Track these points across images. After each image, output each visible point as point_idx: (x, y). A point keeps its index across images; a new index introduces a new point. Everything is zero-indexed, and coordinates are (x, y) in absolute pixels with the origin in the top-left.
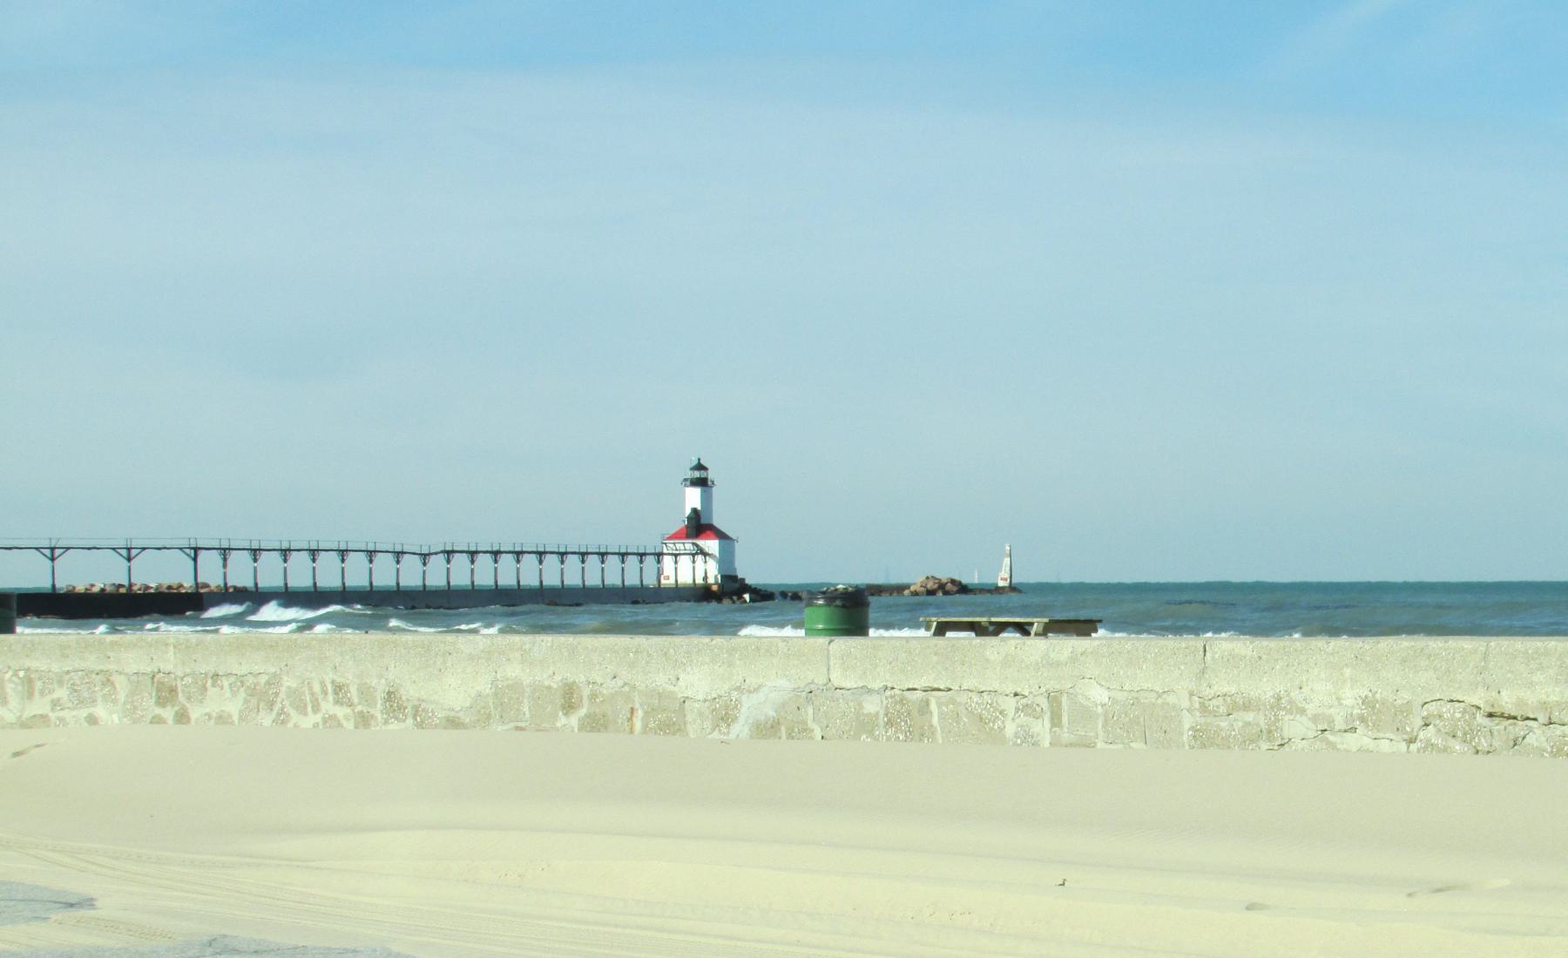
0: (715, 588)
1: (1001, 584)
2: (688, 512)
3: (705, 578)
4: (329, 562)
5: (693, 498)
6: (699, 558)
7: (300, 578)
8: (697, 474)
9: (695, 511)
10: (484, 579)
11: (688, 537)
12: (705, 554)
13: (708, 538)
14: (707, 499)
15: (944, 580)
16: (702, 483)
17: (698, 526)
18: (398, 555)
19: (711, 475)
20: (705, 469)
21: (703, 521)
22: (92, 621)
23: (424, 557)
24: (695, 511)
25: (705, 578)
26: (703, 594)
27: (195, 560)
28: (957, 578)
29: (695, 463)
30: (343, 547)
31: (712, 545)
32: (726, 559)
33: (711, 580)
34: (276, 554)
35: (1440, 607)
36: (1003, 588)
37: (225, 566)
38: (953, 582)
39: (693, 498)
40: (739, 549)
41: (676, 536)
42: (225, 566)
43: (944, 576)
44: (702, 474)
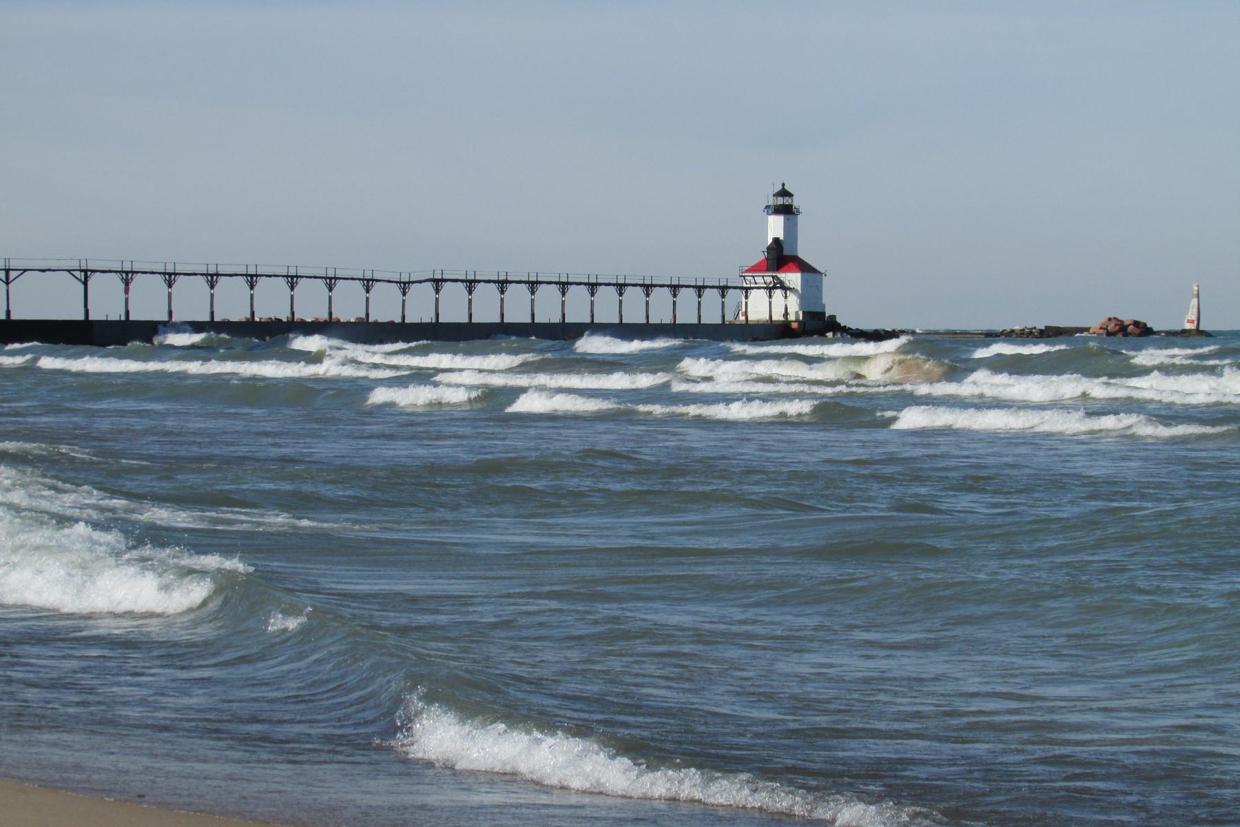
0: (795, 325)
1: (1188, 326)
2: (770, 241)
3: (786, 314)
4: (661, 298)
5: (775, 227)
6: (778, 293)
7: (348, 308)
8: (780, 201)
9: (776, 240)
10: (517, 314)
11: (767, 270)
12: (785, 288)
13: (790, 271)
14: (790, 229)
15: (1126, 323)
16: (786, 210)
17: (780, 257)
18: (471, 284)
19: (796, 202)
20: (790, 195)
21: (786, 252)
22: (80, 348)
23: (405, 286)
24: (776, 240)
25: (786, 314)
26: (780, 331)
27: (85, 283)
28: (1142, 319)
29: (779, 188)
30: (331, 274)
31: (793, 278)
32: (811, 292)
33: (792, 317)
34: (429, 284)
35: (1111, 699)
36: (1189, 331)
37: (127, 291)
38: (1136, 324)
39: (775, 227)
40: (827, 283)
41: (755, 269)
42: (127, 291)
43: (1127, 317)
44: (787, 201)
